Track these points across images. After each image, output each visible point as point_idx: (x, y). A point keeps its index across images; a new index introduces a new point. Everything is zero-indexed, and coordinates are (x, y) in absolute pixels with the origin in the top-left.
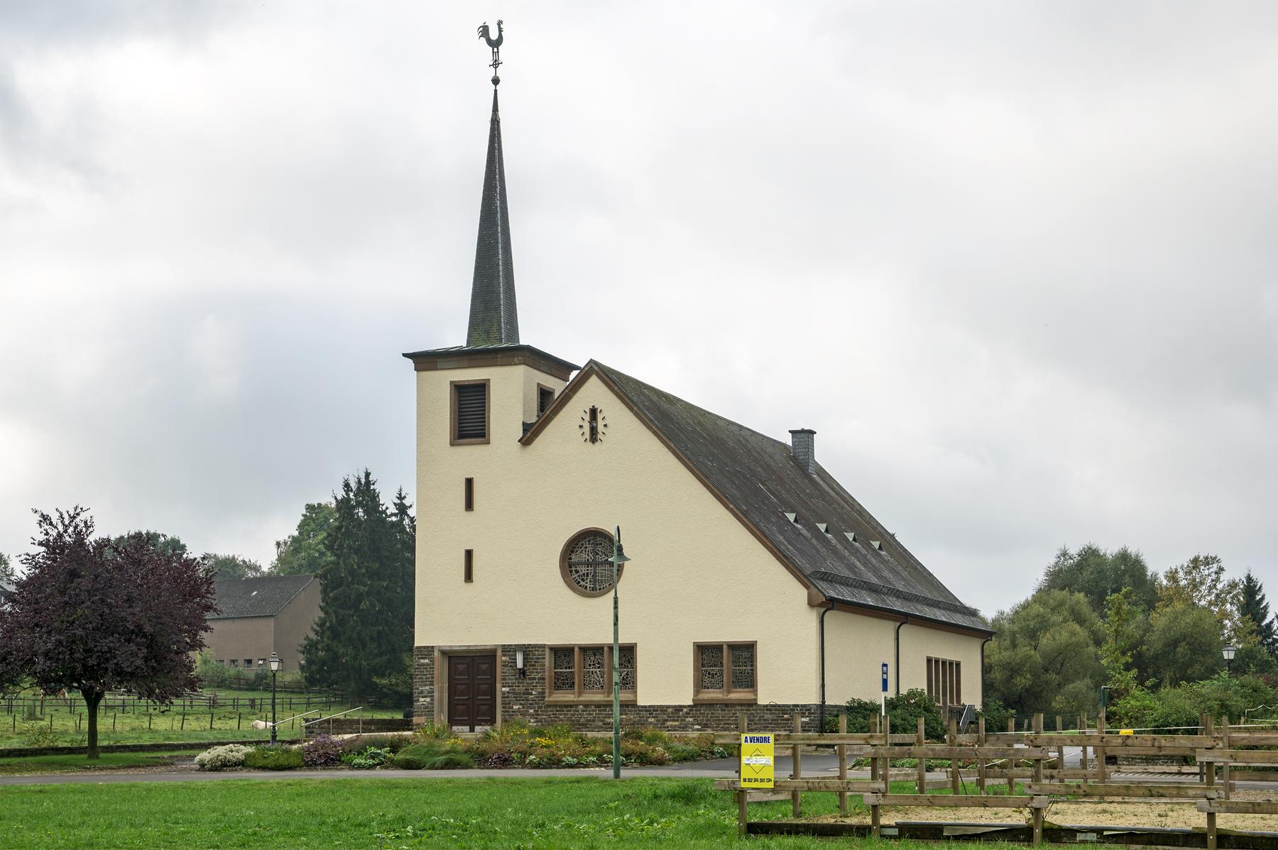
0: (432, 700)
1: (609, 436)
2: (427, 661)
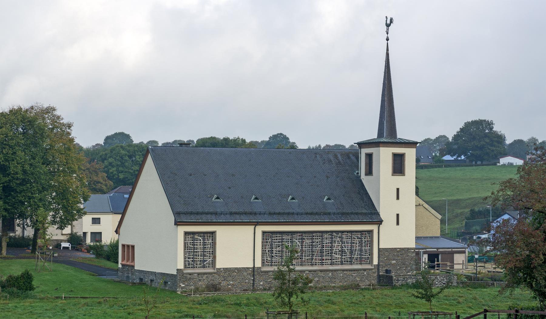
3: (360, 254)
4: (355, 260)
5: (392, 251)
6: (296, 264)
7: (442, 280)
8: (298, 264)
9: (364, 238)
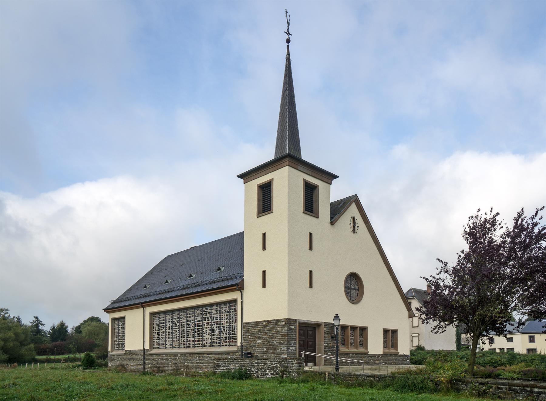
0: (295, 349)
2: (293, 327)
3: (228, 333)
4: (224, 341)
5: (257, 326)
6: (175, 346)
7: (274, 367)
8: (177, 346)
9: (233, 312)
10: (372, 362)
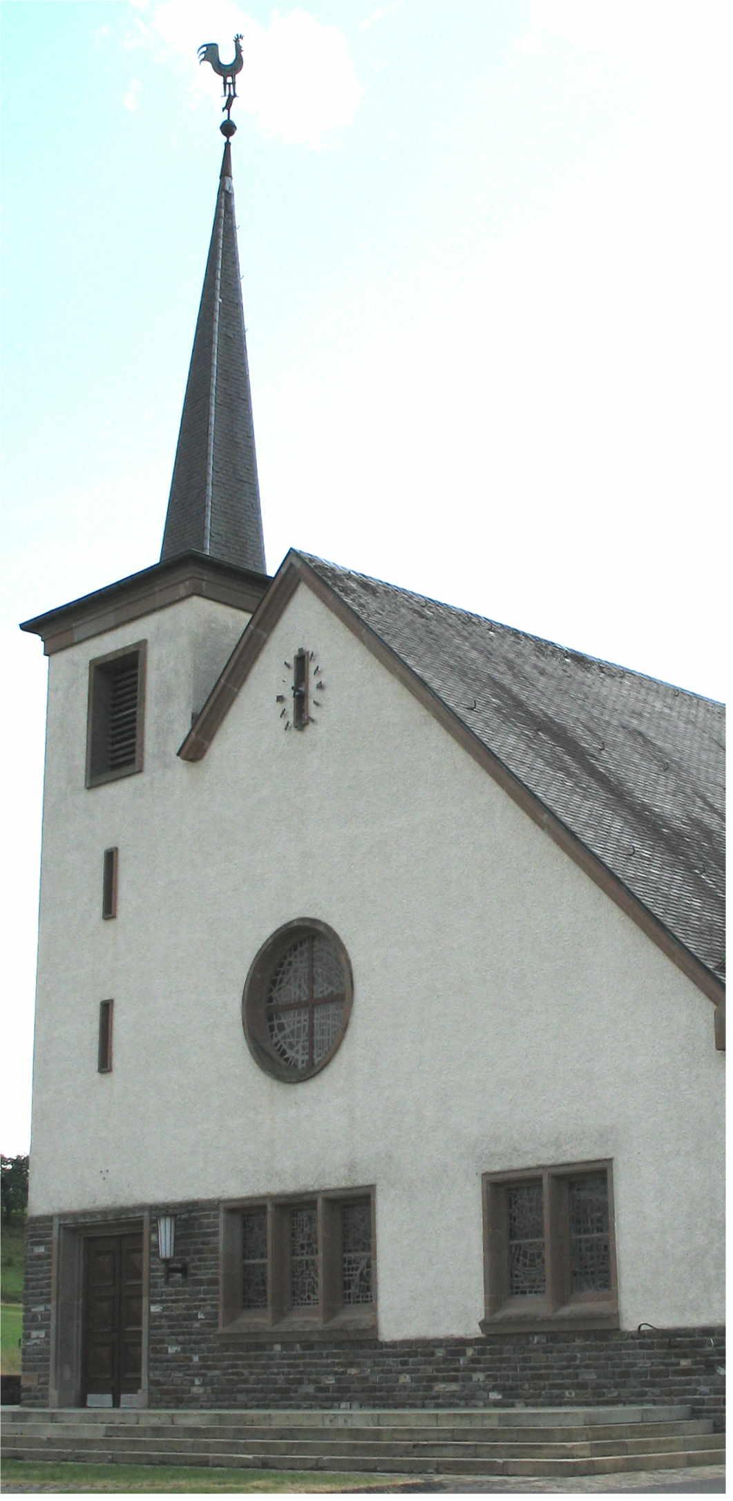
0: (47, 1335)
1: (324, 711)
10: (404, 1387)
